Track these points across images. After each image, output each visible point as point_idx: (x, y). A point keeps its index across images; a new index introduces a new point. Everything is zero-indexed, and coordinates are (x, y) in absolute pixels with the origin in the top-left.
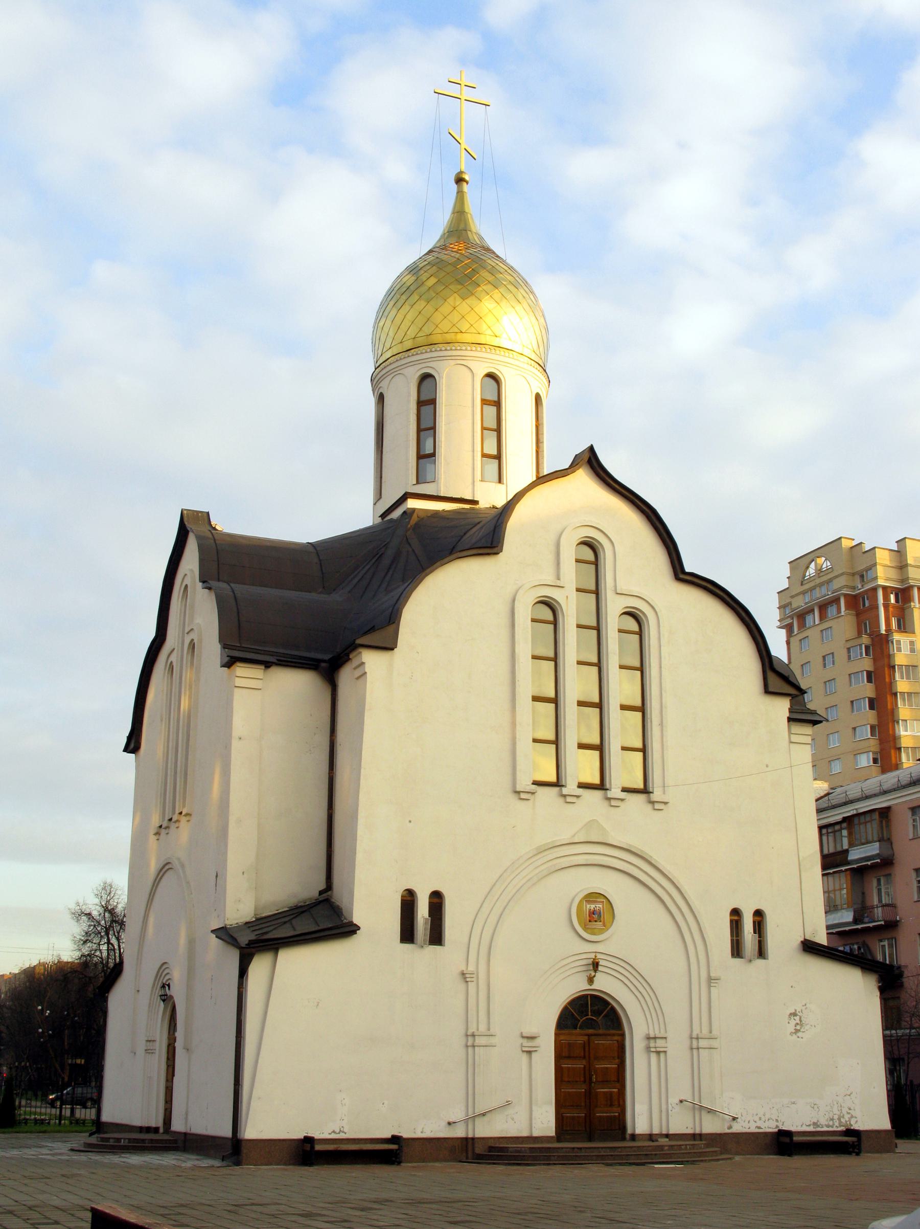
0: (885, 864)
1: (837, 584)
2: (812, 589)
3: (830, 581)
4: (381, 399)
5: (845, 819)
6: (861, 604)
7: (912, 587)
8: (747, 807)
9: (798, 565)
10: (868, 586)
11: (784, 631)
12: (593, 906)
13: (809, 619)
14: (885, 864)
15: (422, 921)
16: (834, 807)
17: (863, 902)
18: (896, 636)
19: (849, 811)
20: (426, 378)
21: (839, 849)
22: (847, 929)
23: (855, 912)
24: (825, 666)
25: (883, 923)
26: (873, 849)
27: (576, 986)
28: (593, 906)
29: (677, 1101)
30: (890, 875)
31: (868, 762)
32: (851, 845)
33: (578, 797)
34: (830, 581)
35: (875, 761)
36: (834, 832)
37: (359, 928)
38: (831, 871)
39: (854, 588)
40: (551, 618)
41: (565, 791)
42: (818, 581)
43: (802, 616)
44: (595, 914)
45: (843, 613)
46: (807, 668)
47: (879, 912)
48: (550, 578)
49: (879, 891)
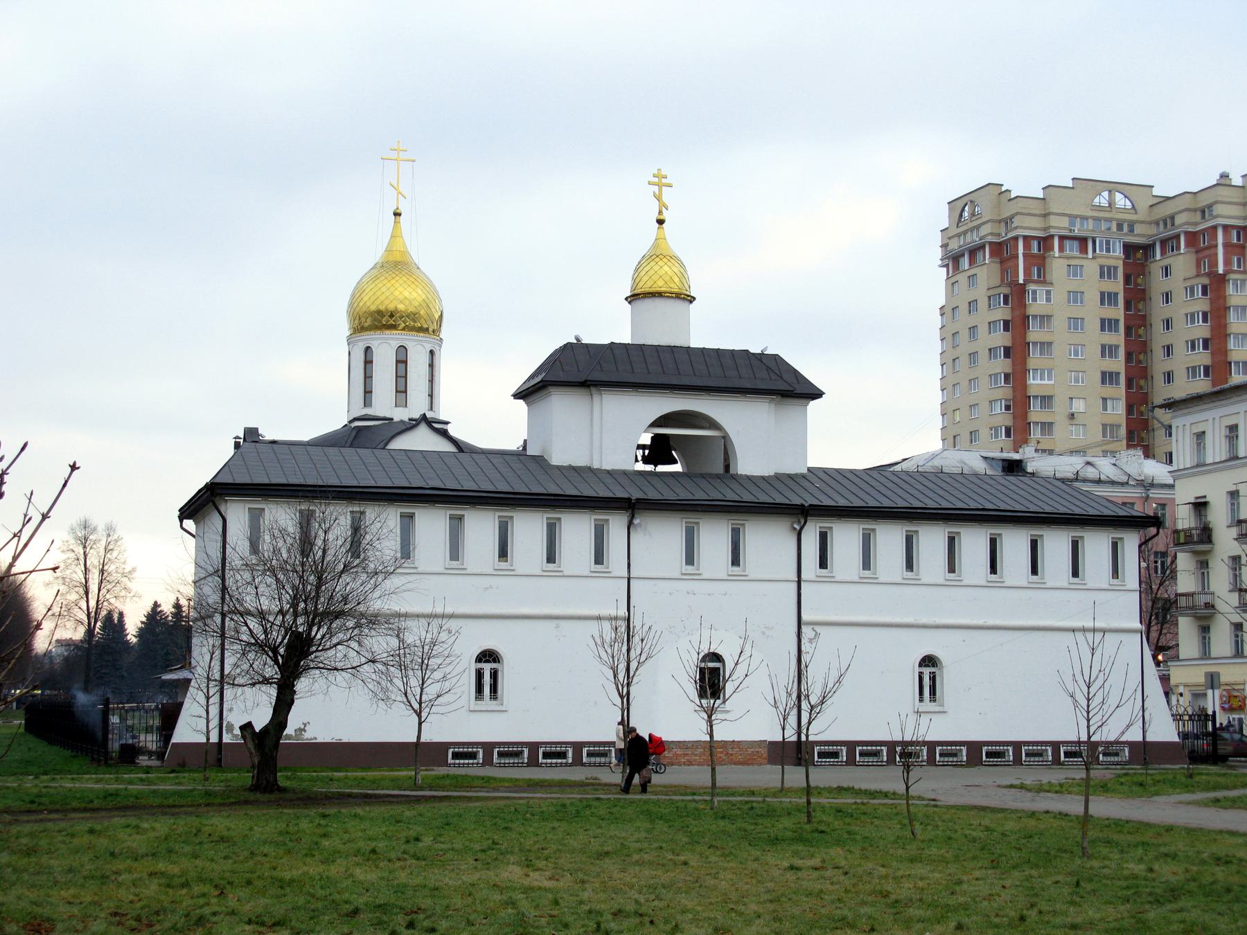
1: (985, 230)
3: (978, 227)
7: (1052, 236)
10: (1010, 235)
18: (1031, 287)
20: (368, 349)
29: (401, 210)
34: (978, 227)
35: (1008, 408)
39: (999, 235)
46: (957, 312)
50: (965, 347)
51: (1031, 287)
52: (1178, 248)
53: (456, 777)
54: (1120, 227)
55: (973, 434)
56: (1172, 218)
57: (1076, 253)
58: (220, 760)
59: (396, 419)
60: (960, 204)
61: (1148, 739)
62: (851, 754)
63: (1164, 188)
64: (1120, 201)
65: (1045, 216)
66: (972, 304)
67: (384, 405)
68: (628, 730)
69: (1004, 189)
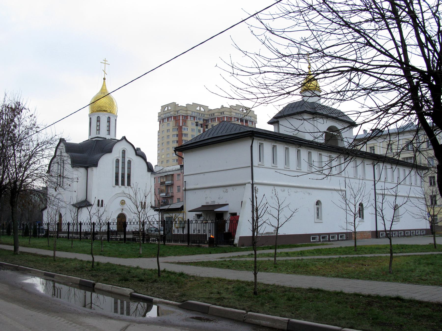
0: (172, 185)
2: (166, 113)
4: (90, 118)
6: (176, 118)
8: (144, 186)
9: (163, 107)
13: (165, 120)
14: (172, 185)
15: (100, 204)
16: (163, 173)
18: (183, 127)
19: (166, 174)
26: (170, 182)
27: (120, 212)
43: (163, 120)
44: (123, 203)
47: (170, 194)
48: (118, 156)
50: (166, 140)
51: (183, 127)
52: (215, 121)
54: (202, 115)
55: (167, 161)
56: (214, 114)
57: (193, 120)
58: (276, 238)
59: (107, 138)
61: (378, 230)
62: (404, 233)
63: (210, 108)
64: (202, 109)
65: (186, 111)
66: (168, 130)
67: (103, 134)
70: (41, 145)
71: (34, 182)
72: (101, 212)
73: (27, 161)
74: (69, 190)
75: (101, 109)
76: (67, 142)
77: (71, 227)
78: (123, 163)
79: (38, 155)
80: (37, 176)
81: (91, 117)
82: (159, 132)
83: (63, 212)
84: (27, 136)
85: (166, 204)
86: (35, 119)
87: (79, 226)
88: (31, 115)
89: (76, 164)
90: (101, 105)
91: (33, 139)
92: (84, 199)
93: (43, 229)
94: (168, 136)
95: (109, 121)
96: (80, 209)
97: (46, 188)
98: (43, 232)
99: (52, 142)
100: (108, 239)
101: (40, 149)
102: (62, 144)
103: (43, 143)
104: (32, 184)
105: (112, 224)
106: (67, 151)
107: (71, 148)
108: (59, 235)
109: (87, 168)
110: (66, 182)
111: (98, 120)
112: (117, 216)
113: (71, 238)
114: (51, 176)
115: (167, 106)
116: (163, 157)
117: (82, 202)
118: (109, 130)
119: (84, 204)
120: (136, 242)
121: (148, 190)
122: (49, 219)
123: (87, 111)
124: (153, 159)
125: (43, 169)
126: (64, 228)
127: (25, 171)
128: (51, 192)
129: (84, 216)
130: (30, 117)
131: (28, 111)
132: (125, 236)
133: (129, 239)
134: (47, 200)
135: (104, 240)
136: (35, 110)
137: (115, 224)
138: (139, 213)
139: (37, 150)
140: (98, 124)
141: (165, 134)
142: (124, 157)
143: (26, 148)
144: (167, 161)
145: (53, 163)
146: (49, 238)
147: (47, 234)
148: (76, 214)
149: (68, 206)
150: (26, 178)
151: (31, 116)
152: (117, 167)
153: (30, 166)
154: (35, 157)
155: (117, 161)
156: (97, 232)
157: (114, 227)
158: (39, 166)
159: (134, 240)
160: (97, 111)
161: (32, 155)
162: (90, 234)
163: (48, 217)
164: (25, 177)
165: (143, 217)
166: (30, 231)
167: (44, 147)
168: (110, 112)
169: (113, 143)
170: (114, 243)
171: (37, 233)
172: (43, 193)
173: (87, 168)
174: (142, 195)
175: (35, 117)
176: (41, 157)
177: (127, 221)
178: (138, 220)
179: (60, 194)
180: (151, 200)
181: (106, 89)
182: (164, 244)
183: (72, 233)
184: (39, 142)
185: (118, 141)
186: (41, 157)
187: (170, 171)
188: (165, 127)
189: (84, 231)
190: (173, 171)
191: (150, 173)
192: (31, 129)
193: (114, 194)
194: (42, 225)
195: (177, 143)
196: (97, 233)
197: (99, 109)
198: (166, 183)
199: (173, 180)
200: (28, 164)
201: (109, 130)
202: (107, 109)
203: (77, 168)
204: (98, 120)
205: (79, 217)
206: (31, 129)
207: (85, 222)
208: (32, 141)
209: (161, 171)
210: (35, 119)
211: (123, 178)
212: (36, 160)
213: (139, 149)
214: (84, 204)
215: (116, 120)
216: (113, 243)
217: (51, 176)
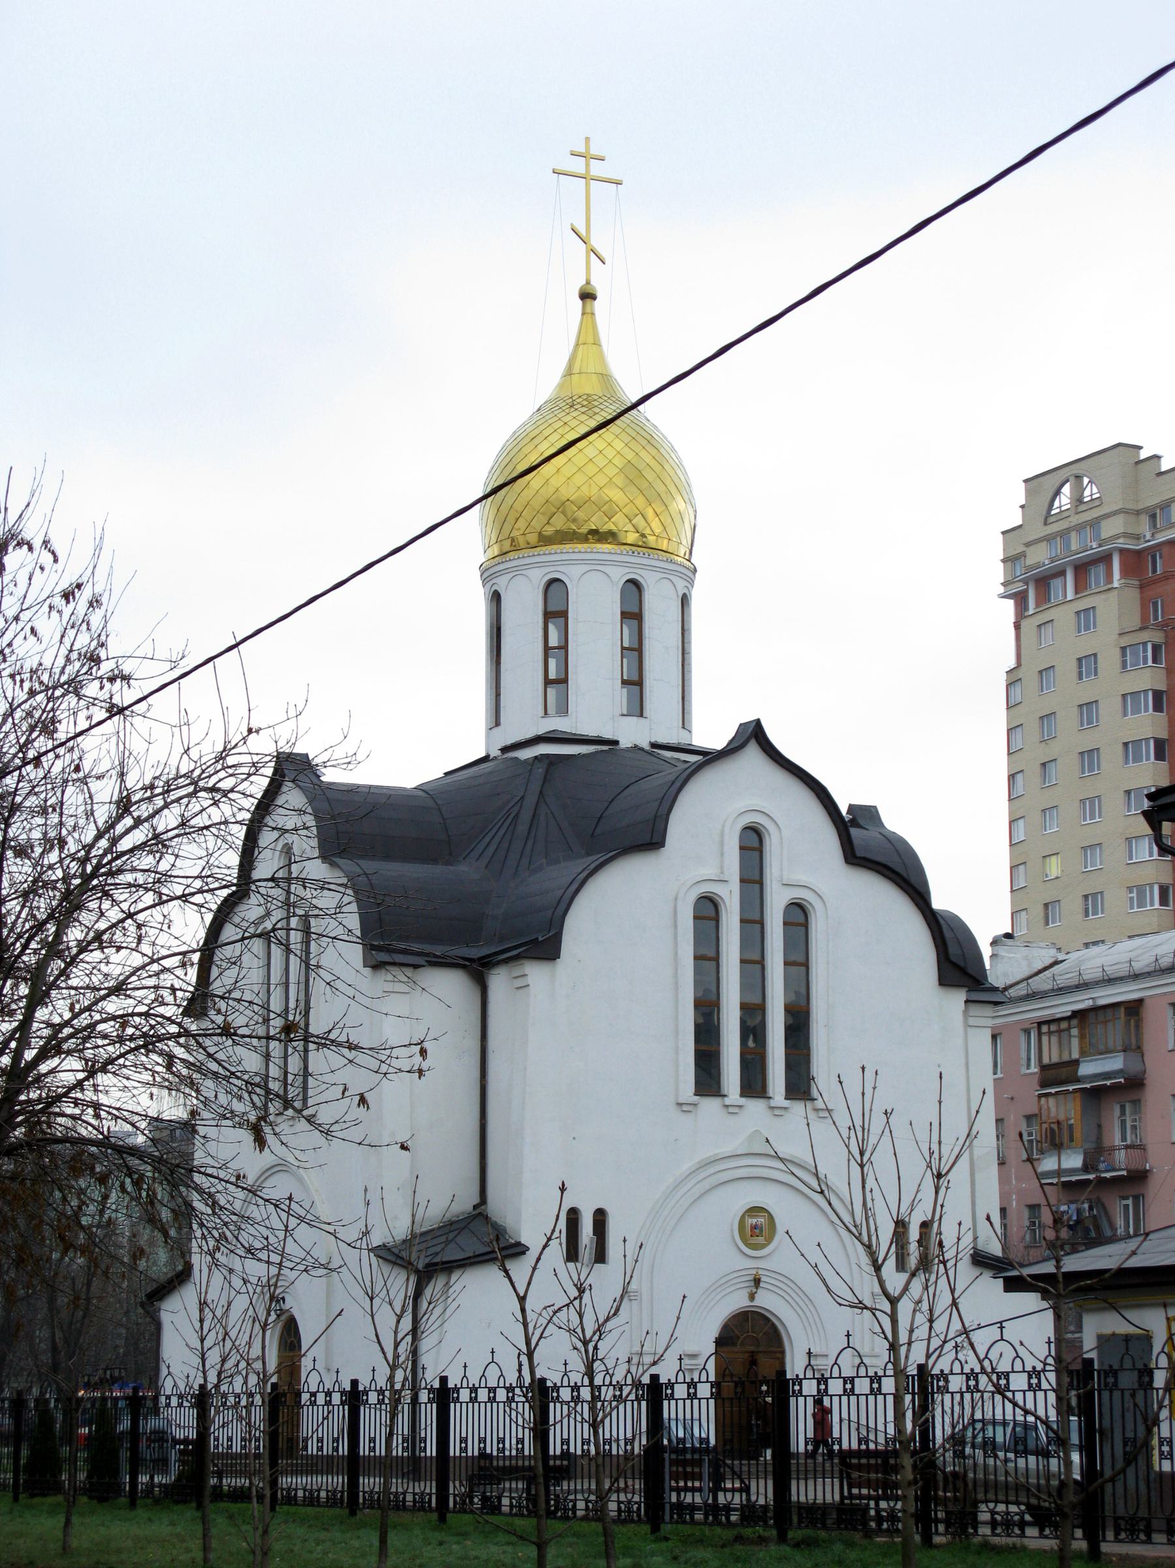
0: (1132, 1086)
2: (1064, 534)
4: (496, 598)
5: (1075, 1014)
8: (918, 1086)
9: (1042, 487)
11: (1010, 603)
12: (754, 1221)
13: (1056, 583)
15: (585, 1237)
17: (1099, 1138)
19: (1082, 1001)
21: (1066, 1058)
22: (1074, 1179)
23: (1085, 1154)
24: (1080, 678)
25: (1124, 1173)
26: (1115, 1063)
27: (738, 1301)
28: (754, 1221)
30: (1139, 1101)
31: (1151, 854)
32: (1083, 1053)
33: (740, 1107)
34: (1095, 523)
36: (1060, 1031)
37: (528, 1249)
38: (1053, 1091)
39: (1137, 537)
40: (713, 914)
41: (727, 1101)
42: (1075, 520)
44: (757, 1228)
45: (1116, 584)
47: (1121, 1157)
48: (710, 871)
49: (1123, 1123)
50: (1070, 738)
53: (904, 1415)
55: (1091, 902)
59: (625, 743)
60: (1051, 483)
66: (1087, 664)
67: (596, 710)
68: (200, 1506)
69: (1143, 455)
70: (144, 810)
71: (101, 1079)
72: (601, 1298)
73: (51, 928)
74: (356, 1134)
75: (574, 526)
76: (330, 776)
77: (372, 1423)
78: (753, 923)
79: (128, 878)
80: (121, 1040)
81: (501, 584)
82: (1013, 679)
83: (307, 1302)
84: (42, 743)
85: (1089, 1233)
86: (96, 618)
87: (429, 1414)
88: (64, 585)
89: (392, 942)
90: (567, 493)
91: (87, 766)
92: (466, 1202)
93: (160, 1436)
94: (1088, 709)
95: (633, 615)
96: (438, 1283)
97: (188, 1127)
98: (162, 1464)
99: (227, 784)
100: (655, 1510)
101: (139, 836)
102: (291, 797)
103: (164, 790)
104: (89, 1095)
105: (681, 1391)
106: (330, 851)
107: (359, 826)
108: (285, 1481)
109: (478, 972)
110: (341, 1077)
111: (555, 612)
112: (713, 1330)
113: (372, 1504)
114: (227, 1031)
115: (1072, 472)
116: (1054, 868)
117: (452, 1228)
118: (635, 683)
119: (461, 1243)
120: (868, 1534)
121: (954, 1129)
122: (214, 1357)
123: (470, 541)
124: (975, 888)
125: (167, 980)
126: (320, 1428)
127: (38, 998)
128: (224, 1152)
129: (476, 1331)
130: (58, 601)
131: (46, 558)
132: (782, 1489)
133: (814, 1514)
134: (185, 1213)
135: (618, 1521)
136: (98, 548)
137: (704, 1390)
138: (893, 1301)
139: (125, 844)
140: (554, 641)
141: (1067, 692)
142: (753, 879)
143: (36, 835)
144: (1091, 902)
145: (229, 932)
146: (211, 1507)
147: (197, 1478)
148: (406, 1324)
149: (351, 1255)
150: (42, 1056)
151: (67, 596)
152: (707, 958)
153: (73, 961)
154: (106, 894)
155: (708, 911)
156: (566, 1455)
157: (695, 1419)
158: (137, 960)
159: (848, 1516)
160: (546, 540)
161: (87, 878)
162: (512, 1471)
163: (194, 1344)
164: (36, 1043)
165: (922, 1332)
166: (65, 1451)
167: (168, 820)
168: (642, 546)
169: (669, 774)
170: (700, 1541)
171: (115, 1472)
172: (169, 1156)
173: (478, 972)
174: (915, 1169)
175: (95, 603)
176: (149, 899)
177: (795, 1366)
178: (878, 1356)
179: (280, 1167)
180: (974, 1207)
181: (606, 378)
182: (1094, 1553)
183: (386, 1466)
184: (130, 781)
185: (710, 758)
186: (149, 899)
187: (1110, 981)
188: (1064, 640)
189: (473, 1450)
190: (1136, 977)
191: (958, 997)
192: (74, 686)
193: (687, 1166)
194: (156, 1411)
195: (1160, 756)
196: (564, 1467)
197: (559, 523)
198: (1085, 1069)
199: (1139, 1049)
200: (54, 948)
201: (635, 683)
202: (618, 523)
203: (409, 972)
204: (555, 612)
205: (425, 1345)
206: (74, 686)
207: (474, 1380)
208: (84, 781)
209: (1042, 983)
210: (96, 618)
211: (753, 1040)
212: (114, 915)
213: (865, 816)
214: (461, 1243)
215: (685, 601)
216: (686, 1540)
217: (227, 1031)
